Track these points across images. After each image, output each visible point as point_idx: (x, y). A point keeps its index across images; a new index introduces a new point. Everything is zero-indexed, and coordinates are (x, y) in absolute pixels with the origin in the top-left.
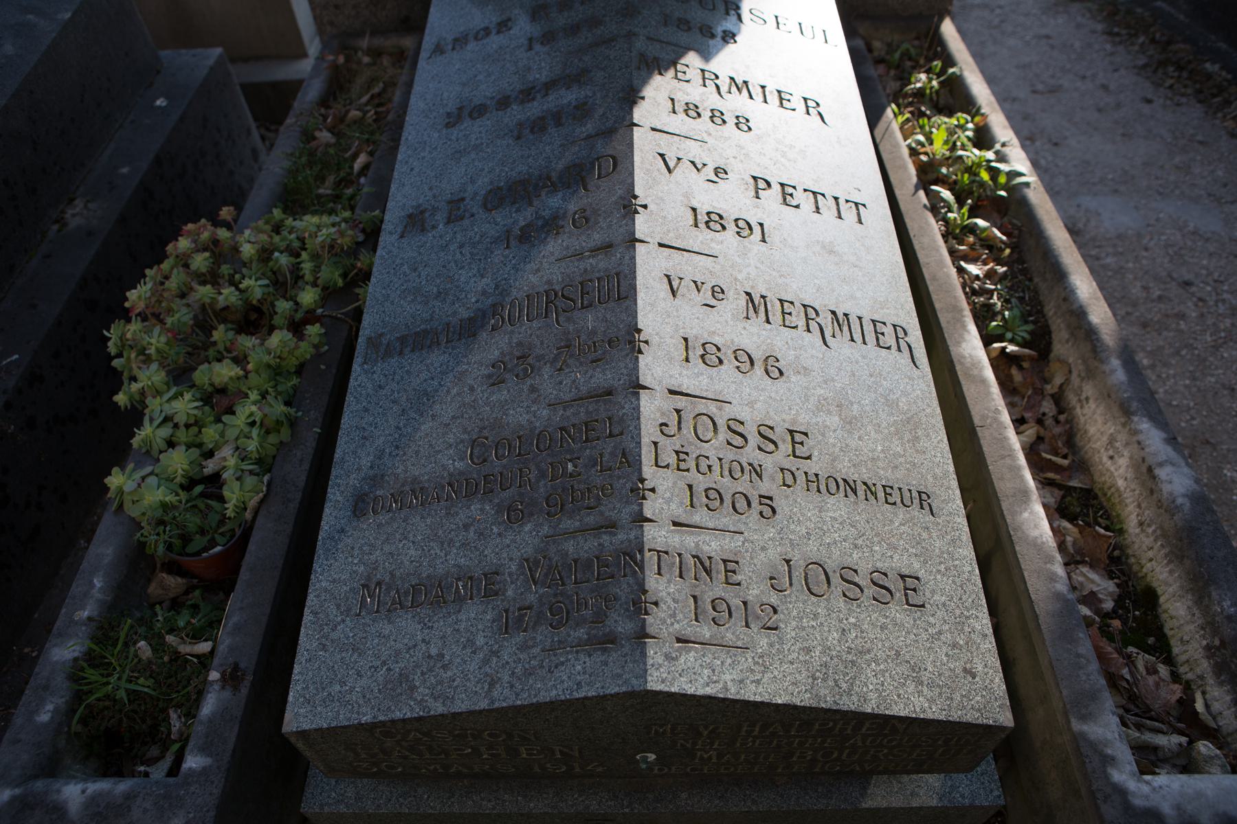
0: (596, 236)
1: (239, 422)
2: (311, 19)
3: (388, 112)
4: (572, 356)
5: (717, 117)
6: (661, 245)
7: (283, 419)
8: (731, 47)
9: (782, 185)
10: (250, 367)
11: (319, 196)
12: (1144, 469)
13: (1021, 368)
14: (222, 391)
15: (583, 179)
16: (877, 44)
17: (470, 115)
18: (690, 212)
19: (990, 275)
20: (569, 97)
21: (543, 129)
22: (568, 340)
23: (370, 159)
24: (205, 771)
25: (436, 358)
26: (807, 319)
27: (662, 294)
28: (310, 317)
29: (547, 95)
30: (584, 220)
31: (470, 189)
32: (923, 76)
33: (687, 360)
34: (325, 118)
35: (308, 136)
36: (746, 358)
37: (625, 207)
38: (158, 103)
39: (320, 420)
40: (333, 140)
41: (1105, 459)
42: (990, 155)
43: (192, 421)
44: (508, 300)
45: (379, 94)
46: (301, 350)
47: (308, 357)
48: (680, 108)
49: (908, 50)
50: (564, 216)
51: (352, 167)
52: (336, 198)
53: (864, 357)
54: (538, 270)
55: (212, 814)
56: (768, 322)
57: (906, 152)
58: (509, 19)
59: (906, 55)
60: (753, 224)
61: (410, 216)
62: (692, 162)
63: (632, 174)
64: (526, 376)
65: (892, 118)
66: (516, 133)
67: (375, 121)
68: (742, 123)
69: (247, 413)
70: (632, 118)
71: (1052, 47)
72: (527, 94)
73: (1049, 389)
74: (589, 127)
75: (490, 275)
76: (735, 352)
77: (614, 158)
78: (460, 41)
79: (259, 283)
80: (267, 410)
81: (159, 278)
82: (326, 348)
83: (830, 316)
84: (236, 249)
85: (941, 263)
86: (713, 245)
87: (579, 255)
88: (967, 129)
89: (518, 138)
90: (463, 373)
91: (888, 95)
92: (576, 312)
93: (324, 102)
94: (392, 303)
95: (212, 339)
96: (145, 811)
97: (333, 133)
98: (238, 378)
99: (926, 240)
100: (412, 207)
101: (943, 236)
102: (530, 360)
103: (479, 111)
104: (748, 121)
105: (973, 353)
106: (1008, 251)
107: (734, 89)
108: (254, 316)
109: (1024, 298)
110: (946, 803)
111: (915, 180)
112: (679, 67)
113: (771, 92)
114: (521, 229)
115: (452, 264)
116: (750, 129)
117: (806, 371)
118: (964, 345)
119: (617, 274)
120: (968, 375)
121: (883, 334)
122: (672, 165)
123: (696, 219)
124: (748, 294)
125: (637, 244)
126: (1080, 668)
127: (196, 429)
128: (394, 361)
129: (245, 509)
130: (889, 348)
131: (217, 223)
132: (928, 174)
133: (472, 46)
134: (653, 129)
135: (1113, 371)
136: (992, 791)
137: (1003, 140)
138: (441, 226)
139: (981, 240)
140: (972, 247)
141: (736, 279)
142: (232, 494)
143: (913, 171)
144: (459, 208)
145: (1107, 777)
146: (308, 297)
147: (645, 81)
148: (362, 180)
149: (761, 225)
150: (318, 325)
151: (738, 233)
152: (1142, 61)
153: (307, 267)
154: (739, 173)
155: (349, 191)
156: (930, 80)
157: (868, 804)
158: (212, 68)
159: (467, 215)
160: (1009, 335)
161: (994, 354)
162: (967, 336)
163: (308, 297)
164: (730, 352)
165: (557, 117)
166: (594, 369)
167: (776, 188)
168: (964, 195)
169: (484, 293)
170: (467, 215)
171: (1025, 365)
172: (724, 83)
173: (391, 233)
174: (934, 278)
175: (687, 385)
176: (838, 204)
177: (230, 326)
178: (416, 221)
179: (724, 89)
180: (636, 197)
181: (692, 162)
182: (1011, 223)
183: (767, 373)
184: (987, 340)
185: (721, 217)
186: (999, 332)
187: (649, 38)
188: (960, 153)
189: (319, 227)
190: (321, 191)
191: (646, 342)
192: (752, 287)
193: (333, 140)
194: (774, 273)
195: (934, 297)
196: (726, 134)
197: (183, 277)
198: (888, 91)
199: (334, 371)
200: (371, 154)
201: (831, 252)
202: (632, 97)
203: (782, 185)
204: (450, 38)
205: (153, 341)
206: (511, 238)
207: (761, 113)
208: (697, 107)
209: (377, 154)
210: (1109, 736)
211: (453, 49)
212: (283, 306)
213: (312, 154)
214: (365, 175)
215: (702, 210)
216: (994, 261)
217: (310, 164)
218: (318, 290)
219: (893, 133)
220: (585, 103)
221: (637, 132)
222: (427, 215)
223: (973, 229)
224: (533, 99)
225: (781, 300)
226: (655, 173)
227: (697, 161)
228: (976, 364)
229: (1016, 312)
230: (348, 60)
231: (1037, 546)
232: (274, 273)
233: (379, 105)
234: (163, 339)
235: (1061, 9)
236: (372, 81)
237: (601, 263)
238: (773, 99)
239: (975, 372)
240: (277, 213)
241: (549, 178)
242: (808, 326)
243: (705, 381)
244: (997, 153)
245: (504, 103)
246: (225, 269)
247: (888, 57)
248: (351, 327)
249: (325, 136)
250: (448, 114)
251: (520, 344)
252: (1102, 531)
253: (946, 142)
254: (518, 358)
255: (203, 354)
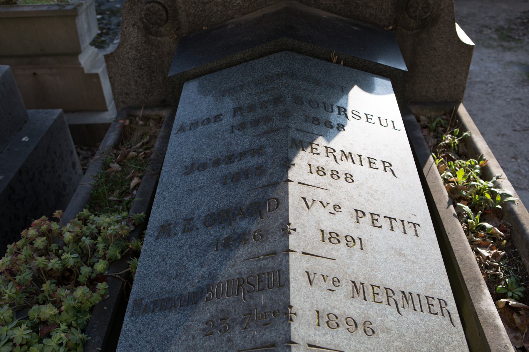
0: (267, 247)
1: (53, 344)
2: (111, 91)
3: (151, 153)
4: (252, 320)
5: (335, 174)
6: (303, 253)
7: (80, 342)
8: (342, 133)
9: (372, 214)
10: (63, 308)
11: (110, 201)
13: (519, 314)
14: (45, 323)
15: (260, 211)
16: (422, 118)
17: (198, 169)
18: (321, 233)
19: (495, 256)
20: (253, 162)
21: (238, 180)
22: (250, 310)
23: (140, 181)
25: (174, 316)
26: (388, 297)
27: (304, 284)
28: (101, 278)
29: (240, 160)
30: (261, 236)
31: (197, 213)
32: (449, 136)
33: (319, 325)
34: (116, 156)
35: (106, 166)
36: (353, 323)
37: (283, 230)
38: (24, 139)
39: (101, 342)
40: (120, 169)
42: (490, 184)
44: (216, 282)
45: (147, 143)
46: (94, 298)
47: (97, 302)
48: (314, 170)
49: (440, 121)
50: (249, 233)
51: (129, 185)
52: (120, 202)
53: (422, 320)
54: (234, 266)
56: (365, 299)
57: (441, 181)
58: (221, 115)
59: (439, 125)
60: (356, 239)
61: (162, 226)
62: (321, 202)
63: (287, 210)
64: (225, 331)
65: (432, 163)
66: (223, 181)
67: (143, 158)
68: (349, 178)
69: (59, 337)
70: (288, 176)
71: (523, 105)
72: (230, 158)
74: (264, 180)
75: (206, 266)
76: (346, 319)
77: (277, 200)
78: (194, 125)
79: (73, 256)
80: (71, 337)
81: (15, 250)
82: (108, 296)
83: (401, 295)
84: (61, 234)
85: (465, 250)
86: (333, 252)
87: (257, 257)
88: (476, 168)
89: (225, 184)
90: (189, 327)
91: (430, 147)
92: (255, 293)
93: (116, 146)
94: (150, 279)
95: (42, 289)
97: (120, 165)
98: (55, 315)
99: (456, 236)
100: (164, 221)
101: (465, 232)
102: (228, 321)
103: (203, 167)
104: (352, 176)
105: (489, 308)
106: (505, 242)
107: (344, 158)
108: (67, 274)
109: (517, 270)
111: (447, 199)
112: (313, 145)
113: (364, 159)
114: (225, 239)
115: (185, 258)
116: (353, 181)
117: (388, 330)
118: (482, 303)
119: (279, 271)
120: (486, 322)
121: (432, 305)
122: (309, 204)
123: (323, 237)
124: (353, 282)
125: (290, 253)
127: (26, 347)
128: (149, 316)
130: (436, 314)
131: (52, 219)
132: (455, 195)
133: (200, 128)
134: (299, 183)
137: (497, 175)
138: (179, 234)
139: (488, 234)
140: (483, 238)
141: (346, 273)
143: (446, 194)
144: (190, 224)
146: (100, 266)
147: (295, 155)
148: (135, 192)
149: (360, 239)
150: (104, 283)
151: (347, 244)
153: (101, 246)
154: (347, 208)
155: (127, 199)
156: (454, 139)
158: (55, 120)
159: (195, 229)
160: (510, 294)
161: (502, 306)
162: (483, 297)
163: (100, 266)
164: (343, 319)
165: (246, 173)
166: (265, 330)
167: (368, 216)
168: (476, 207)
169: (203, 277)
170: (195, 229)
171: (522, 312)
172: (338, 154)
173: (150, 236)
174: (462, 260)
175: (319, 340)
176: (403, 225)
177: (53, 281)
178: (166, 230)
179: (338, 158)
180: (289, 224)
181: (321, 202)
182: (505, 224)
183: (365, 332)
184: (496, 297)
185: (337, 235)
186: (504, 291)
187: (297, 130)
188: (473, 183)
189: (110, 224)
190: (111, 198)
191: (295, 314)
192: (356, 278)
193: (120, 169)
194: (368, 269)
195: (463, 272)
196: (340, 185)
197: (29, 252)
198: (430, 144)
199: (112, 311)
200: (141, 178)
201: (400, 254)
202: (287, 164)
203: (372, 214)
204: (188, 123)
205: (7, 291)
206: (219, 245)
207: (359, 172)
208: (323, 169)
209: (144, 178)
211: (190, 129)
212: (85, 270)
213: (107, 176)
214: (137, 190)
215: (327, 231)
216: (497, 248)
217: (106, 182)
218: (106, 262)
219: (434, 170)
220: (262, 166)
221: (291, 185)
222: (172, 227)
223: (483, 228)
224: (233, 162)
225: (372, 286)
226: (301, 210)
227: (324, 202)
228: (490, 316)
229: (513, 279)
230: (130, 123)
232: (82, 249)
233: (146, 149)
234: (14, 291)
235: (526, 84)
236: (142, 137)
237: (269, 263)
238: (366, 162)
239: (491, 321)
240: (86, 212)
241: (241, 210)
242: (388, 301)
243: (329, 338)
244: (494, 182)
245: (217, 163)
246: (54, 246)
247: (429, 125)
248: (124, 283)
249: (115, 166)
250: (186, 167)
251: (222, 311)
253: (464, 177)
254: (221, 320)
255: (35, 297)
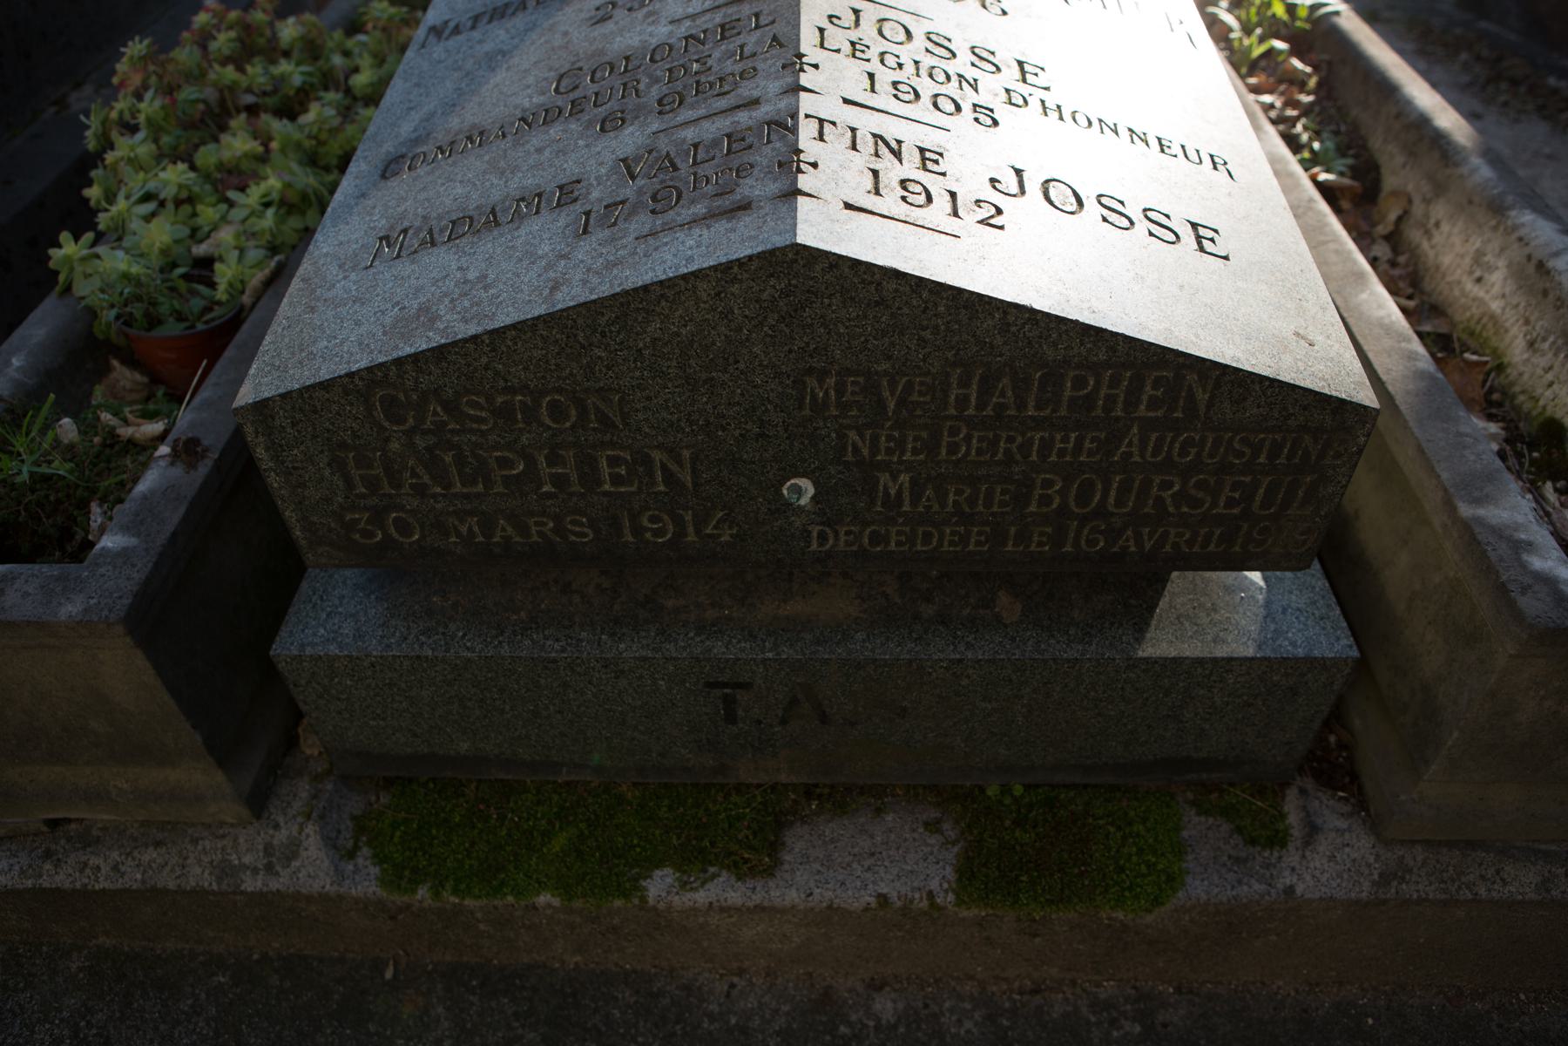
12: (1531, 269)
24: (124, 553)
41: (1469, 286)
43: (184, 194)
55: (127, 601)
73: (1381, 230)
96: (26, 595)
110: (1269, 653)
126: (1465, 447)
129: (243, 292)
134: (846, 101)
135: (1474, 171)
136: (1338, 639)
142: (224, 273)
145: (1524, 566)
152: (1465, 79)
157: (1147, 651)
210: (1520, 519)
229: (1330, 144)
231: (1388, 329)
252: (1475, 358)
